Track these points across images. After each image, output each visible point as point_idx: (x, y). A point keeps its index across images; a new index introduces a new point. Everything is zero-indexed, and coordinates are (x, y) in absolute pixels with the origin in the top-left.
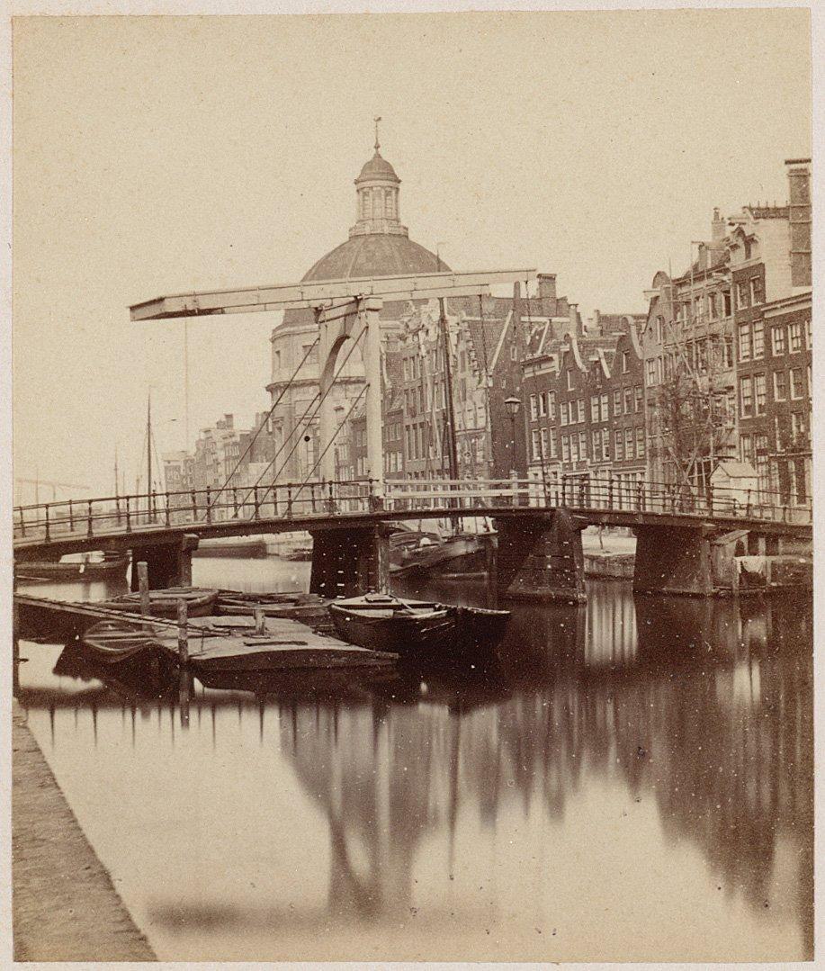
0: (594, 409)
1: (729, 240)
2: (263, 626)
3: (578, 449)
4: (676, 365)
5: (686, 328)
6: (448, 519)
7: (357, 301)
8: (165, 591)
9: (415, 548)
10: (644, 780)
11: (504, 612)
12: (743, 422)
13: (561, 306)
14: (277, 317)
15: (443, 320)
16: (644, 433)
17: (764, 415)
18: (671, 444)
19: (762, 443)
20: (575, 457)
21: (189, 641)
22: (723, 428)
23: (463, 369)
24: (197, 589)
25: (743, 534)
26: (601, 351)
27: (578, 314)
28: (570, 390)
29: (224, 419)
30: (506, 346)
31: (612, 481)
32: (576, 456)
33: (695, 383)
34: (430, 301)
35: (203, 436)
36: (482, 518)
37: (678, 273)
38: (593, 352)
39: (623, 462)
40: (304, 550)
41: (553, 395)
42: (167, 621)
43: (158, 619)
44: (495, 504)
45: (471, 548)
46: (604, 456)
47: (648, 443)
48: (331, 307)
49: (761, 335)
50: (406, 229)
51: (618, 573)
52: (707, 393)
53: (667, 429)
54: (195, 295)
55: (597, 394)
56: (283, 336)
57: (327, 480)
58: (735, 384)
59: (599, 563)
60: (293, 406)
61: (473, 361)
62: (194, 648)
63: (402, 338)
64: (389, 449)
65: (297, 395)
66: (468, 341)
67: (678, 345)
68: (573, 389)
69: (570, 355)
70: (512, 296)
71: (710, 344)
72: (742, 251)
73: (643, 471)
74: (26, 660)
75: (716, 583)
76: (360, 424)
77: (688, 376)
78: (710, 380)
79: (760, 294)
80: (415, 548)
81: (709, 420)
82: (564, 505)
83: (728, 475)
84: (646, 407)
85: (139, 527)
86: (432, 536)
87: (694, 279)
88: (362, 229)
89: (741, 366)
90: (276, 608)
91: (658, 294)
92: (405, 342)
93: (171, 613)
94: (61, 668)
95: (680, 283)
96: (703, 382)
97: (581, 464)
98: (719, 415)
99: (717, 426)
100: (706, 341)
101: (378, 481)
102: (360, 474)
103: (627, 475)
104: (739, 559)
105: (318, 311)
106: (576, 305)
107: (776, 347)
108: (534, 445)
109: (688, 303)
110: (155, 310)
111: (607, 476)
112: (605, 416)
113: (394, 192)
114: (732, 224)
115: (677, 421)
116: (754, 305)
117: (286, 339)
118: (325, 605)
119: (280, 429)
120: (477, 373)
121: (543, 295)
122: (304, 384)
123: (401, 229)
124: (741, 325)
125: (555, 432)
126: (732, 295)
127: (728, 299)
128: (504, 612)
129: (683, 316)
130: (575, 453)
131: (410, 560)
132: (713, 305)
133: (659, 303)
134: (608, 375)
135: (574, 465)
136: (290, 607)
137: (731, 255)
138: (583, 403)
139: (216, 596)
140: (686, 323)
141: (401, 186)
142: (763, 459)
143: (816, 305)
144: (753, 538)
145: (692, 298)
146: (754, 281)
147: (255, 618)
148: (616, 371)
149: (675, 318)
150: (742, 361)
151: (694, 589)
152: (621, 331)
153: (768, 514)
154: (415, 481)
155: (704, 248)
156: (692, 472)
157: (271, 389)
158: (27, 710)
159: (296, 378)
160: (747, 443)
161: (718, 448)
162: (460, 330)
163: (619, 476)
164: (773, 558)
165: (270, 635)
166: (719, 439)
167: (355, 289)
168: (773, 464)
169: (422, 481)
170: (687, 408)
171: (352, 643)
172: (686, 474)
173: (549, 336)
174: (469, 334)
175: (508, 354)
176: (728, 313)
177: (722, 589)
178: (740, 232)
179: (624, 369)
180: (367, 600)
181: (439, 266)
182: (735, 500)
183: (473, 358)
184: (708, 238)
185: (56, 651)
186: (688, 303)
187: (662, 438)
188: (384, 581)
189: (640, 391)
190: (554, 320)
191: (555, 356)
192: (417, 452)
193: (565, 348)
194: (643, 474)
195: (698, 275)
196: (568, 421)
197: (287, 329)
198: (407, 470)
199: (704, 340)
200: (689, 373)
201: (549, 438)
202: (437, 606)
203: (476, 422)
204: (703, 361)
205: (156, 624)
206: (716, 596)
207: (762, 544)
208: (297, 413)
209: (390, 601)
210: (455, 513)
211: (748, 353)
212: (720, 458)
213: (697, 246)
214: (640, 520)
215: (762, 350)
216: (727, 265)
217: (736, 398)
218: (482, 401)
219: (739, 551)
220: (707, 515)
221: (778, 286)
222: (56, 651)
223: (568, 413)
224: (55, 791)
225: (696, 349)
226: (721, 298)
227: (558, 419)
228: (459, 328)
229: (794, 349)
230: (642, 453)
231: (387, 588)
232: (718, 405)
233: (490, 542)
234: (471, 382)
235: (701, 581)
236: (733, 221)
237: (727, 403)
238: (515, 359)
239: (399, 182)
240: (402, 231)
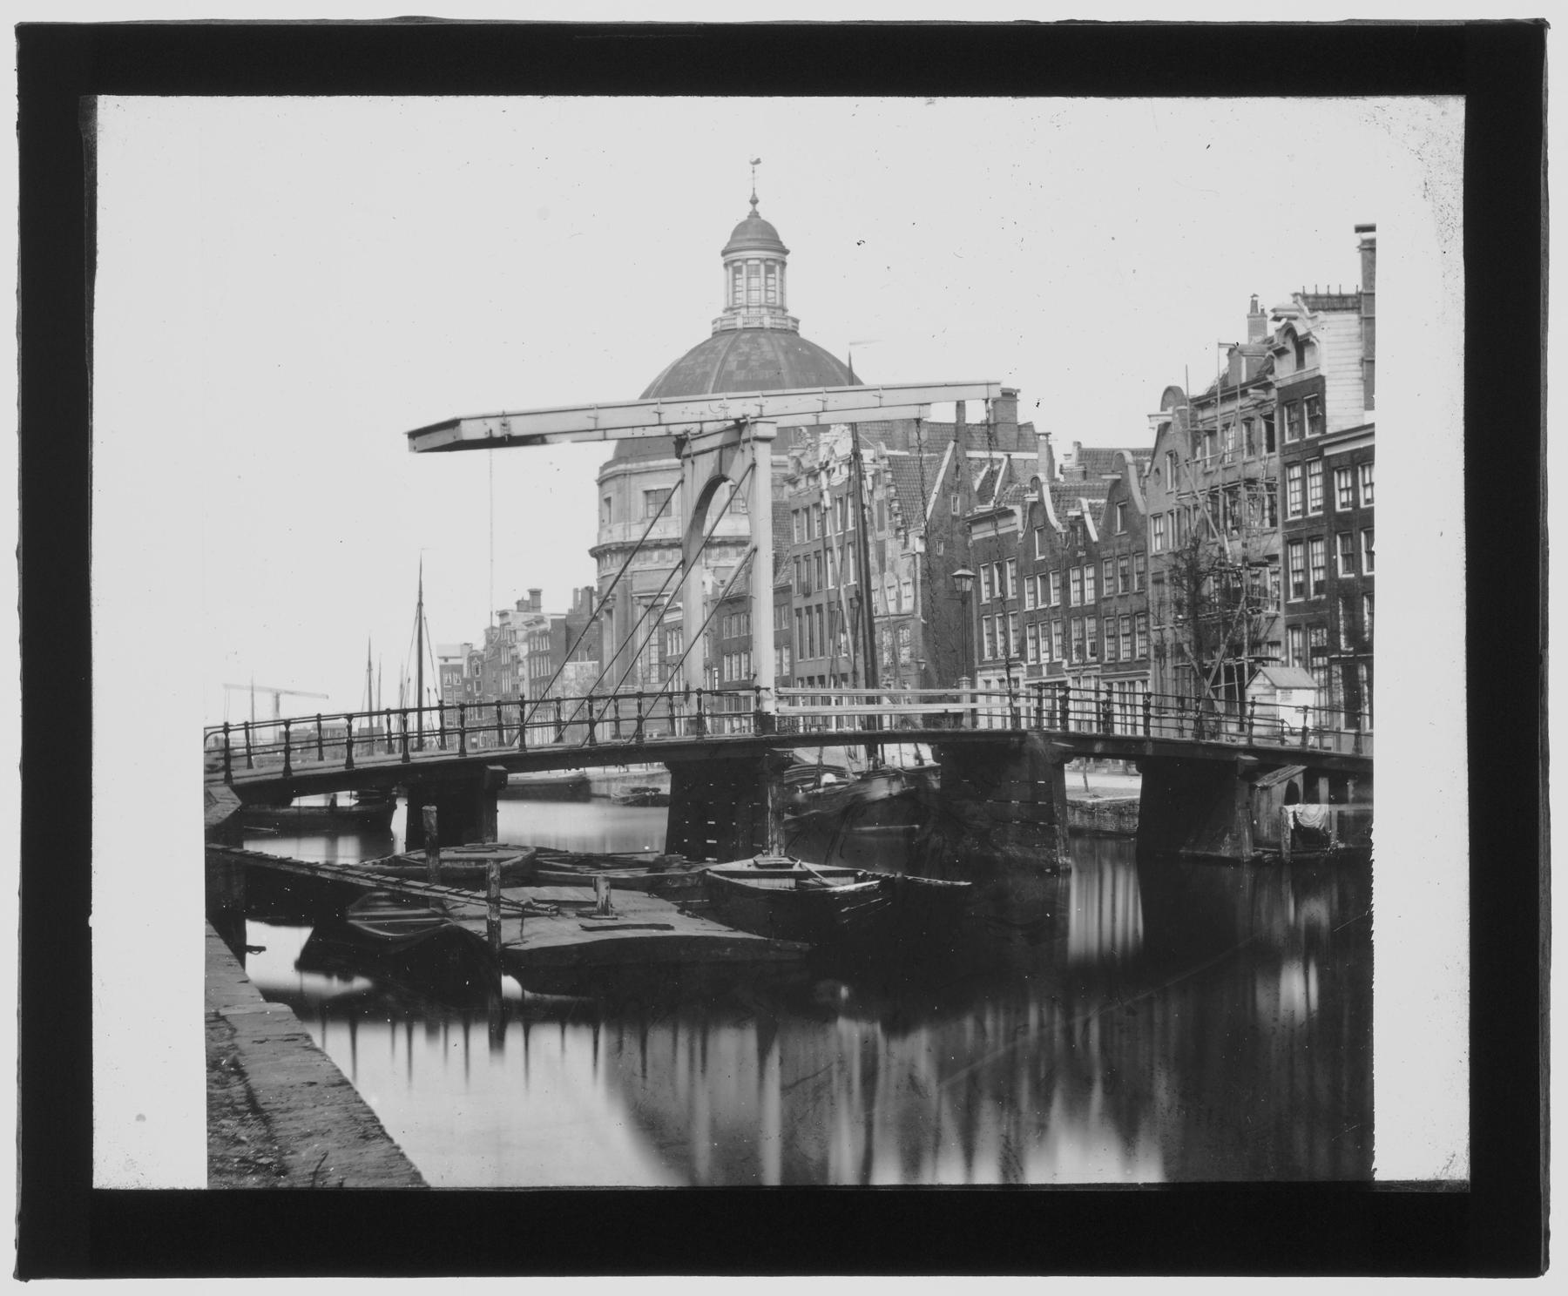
0: (1074, 587)
1: (1272, 342)
2: (607, 901)
3: (1050, 644)
4: (1194, 524)
5: (1209, 469)
6: (862, 747)
7: (739, 425)
8: (458, 848)
9: (814, 787)
10: (1144, 1125)
11: (962, 883)
12: (1291, 608)
13: (1026, 436)
14: (607, 451)
15: (856, 455)
16: (1147, 624)
17: (1324, 597)
18: (1186, 637)
19: (1318, 638)
20: (1045, 657)
21: (504, 923)
22: (1263, 616)
23: (882, 528)
24: (505, 847)
25: (1296, 772)
26: (1085, 502)
27: (1050, 448)
28: (1039, 558)
29: (527, 597)
30: (945, 493)
31: (1097, 692)
32: (1047, 656)
33: (1222, 549)
34: (832, 426)
35: (497, 622)
36: (912, 745)
37: (1198, 389)
38: (1074, 504)
39: (1115, 664)
40: (647, 790)
41: (1014, 566)
42: (467, 892)
43: (454, 891)
44: (926, 725)
45: (896, 788)
46: (1088, 656)
47: (1154, 636)
48: (701, 435)
49: (1318, 481)
50: (796, 321)
51: (1110, 826)
52: (1239, 565)
53: (1180, 617)
54: (504, 415)
55: (1078, 564)
56: (614, 477)
57: (694, 687)
58: (1280, 552)
59: (1083, 812)
60: (629, 578)
61: (896, 515)
62: (510, 932)
63: (793, 481)
64: (782, 641)
65: (653, 561)
66: (889, 486)
67: (1198, 494)
68: (1043, 557)
69: (1040, 507)
70: (953, 420)
71: (1244, 493)
72: (1292, 357)
73: (1143, 678)
74: (261, 949)
75: (1257, 842)
76: (734, 604)
77: (1211, 540)
78: (1245, 545)
79: (1318, 421)
80: (814, 787)
81: (1243, 605)
82: (1039, 726)
83: (1273, 684)
84: (1150, 584)
85: (432, 752)
86: (838, 771)
87: (1222, 398)
88: (733, 322)
89: (1287, 525)
90: (623, 874)
91: (1169, 419)
92: (795, 488)
93: (474, 879)
94: (307, 962)
95: (1202, 403)
96: (1233, 548)
97: (1054, 667)
98: (1256, 597)
99: (1253, 613)
100: (1239, 489)
101: (767, 689)
102: (726, 679)
103: (1122, 684)
104: (1290, 809)
105: (681, 442)
106: (1047, 435)
107: (1342, 498)
108: (986, 638)
109: (1212, 433)
110: (446, 437)
111: (1092, 684)
112: (1090, 595)
113: (778, 268)
114: (1277, 319)
115: (1196, 603)
116: (1308, 436)
117: (620, 480)
118: (694, 871)
119: (609, 612)
120: (902, 533)
121: (999, 419)
122: (658, 545)
123: (789, 321)
124: (1290, 465)
125: (1016, 619)
126: (1276, 422)
127: (1270, 428)
128: (962, 883)
129: (1205, 452)
130: (1044, 651)
131: (805, 807)
132: (1249, 436)
133: (1171, 432)
134: (1095, 537)
135: (1044, 669)
136: (642, 873)
137: (1276, 363)
138: (1057, 577)
139: (533, 857)
140: (1208, 462)
141: (788, 258)
142: (1320, 661)
143: (1380, 443)
144: (1311, 780)
145: (1218, 425)
146: (1308, 401)
147: (596, 890)
148: (1107, 531)
149: (1194, 455)
150: (1290, 518)
151: (1226, 852)
152: (1113, 472)
153: (1329, 742)
154: (810, 690)
155: (1236, 353)
156: (1217, 680)
157: (599, 553)
158: (324, 1029)
159: (649, 537)
160: (1297, 639)
161: (1255, 644)
162: (876, 470)
163: (1110, 685)
164: (1343, 808)
165: (617, 914)
166: (1256, 632)
167: (739, 407)
168: (1334, 668)
169: (819, 690)
170: (1210, 586)
171: (737, 928)
172: (1207, 683)
173: (1007, 479)
174: (889, 476)
175: (947, 505)
176: (1271, 448)
177: (1265, 853)
178: (1289, 331)
179: (1119, 529)
180: (756, 864)
181: (847, 377)
182: (1283, 721)
183: (896, 510)
184: (1241, 336)
185: (301, 936)
186: (1212, 433)
187: (1171, 628)
188: (775, 837)
189: (1141, 560)
190: (1015, 455)
191: (1018, 509)
192: (811, 649)
193: (1032, 497)
194: (1144, 682)
195: (1226, 391)
196: (1036, 604)
197: (622, 467)
198: (797, 674)
199: (1235, 487)
200: (1214, 536)
201: (994, 630)
202: (860, 874)
203: (899, 605)
204: (1233, 518)
205: (450, 897)
206: (1256, 862)
207: (1323, 787)
208: (635, 590)
209: (791, 866)
210: (872, 737)
211: (1299, 507)
212: (1259, 660)
213: (1226, 351)
214: (1149, 751)
215: (1319, 503)
216: (1270, 378)
217: (1282, 571)
218: (909, 575)
219: (1291, 797)
220: (1243, 742)
221: (1341, 411)
222: (301, 936)
223: (1035, 592)
224: (386, 1145)
225: (1224, 499)
226: (1260, 426)
227: (1021, 600)
228: (876, 466)
229: (1343, 505)
230: (1144, 651)
231: (780, 847)
232: (1257, 582)
233: (926, 781)
234: (893, 547)
235: (1237, 839)
236: (1280, 314)
237: (1269, 579)
238: (957, 513)
239: (786, 252)
240: (790, 325)
